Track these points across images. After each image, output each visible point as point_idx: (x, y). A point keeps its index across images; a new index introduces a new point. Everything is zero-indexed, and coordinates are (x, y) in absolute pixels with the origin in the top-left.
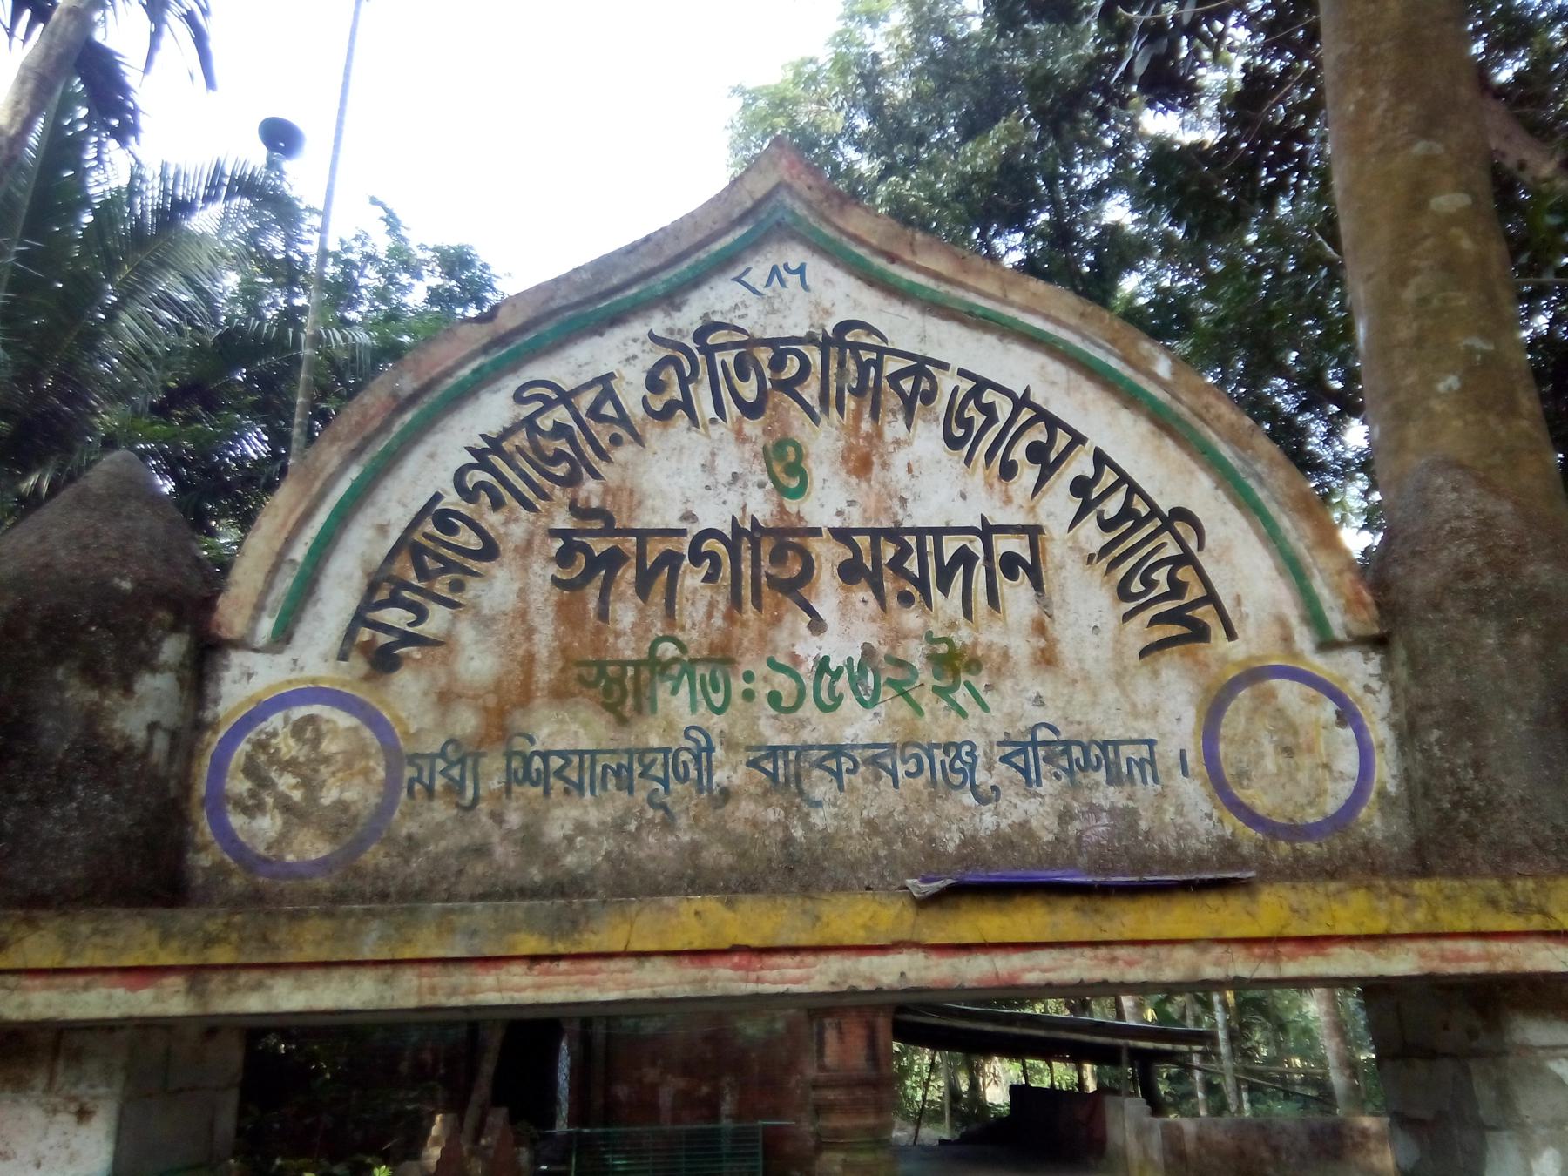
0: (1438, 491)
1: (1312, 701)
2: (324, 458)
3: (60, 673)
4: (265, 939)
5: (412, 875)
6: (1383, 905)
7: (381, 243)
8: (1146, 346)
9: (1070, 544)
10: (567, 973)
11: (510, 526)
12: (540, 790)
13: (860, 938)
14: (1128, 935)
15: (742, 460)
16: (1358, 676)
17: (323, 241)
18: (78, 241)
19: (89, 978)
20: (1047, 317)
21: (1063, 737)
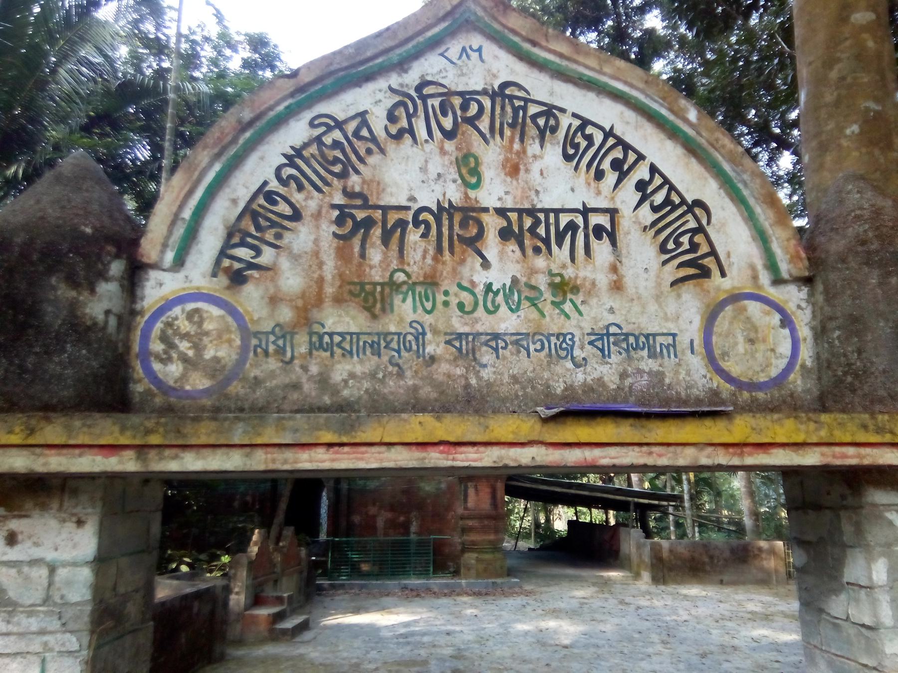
0: (849, 193)
1: (768, 313)
2: (199, 158)
3: (53, 281)
4: (179, 432)
5: (257, 399)
6: (803, 427)
7: (213, 31)
8: (683, 102)
9: (634, 220)
10: (348, 453)
11: (308, 201)
12: (328, 354)
13: (510, 438)
14: (660, 440)
15: (444, 165)
16: (794, 299)
17: (178, 27)
18: (32, 24)
19: (82, 450)
20: (626, 83)
21: (624, 331)
